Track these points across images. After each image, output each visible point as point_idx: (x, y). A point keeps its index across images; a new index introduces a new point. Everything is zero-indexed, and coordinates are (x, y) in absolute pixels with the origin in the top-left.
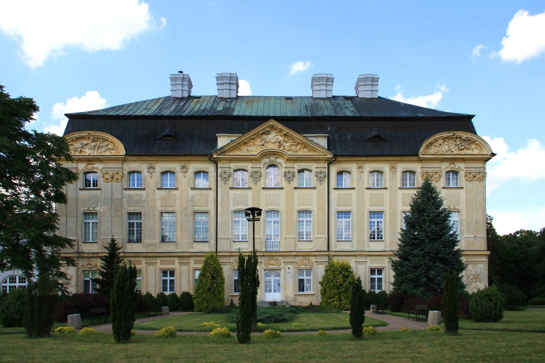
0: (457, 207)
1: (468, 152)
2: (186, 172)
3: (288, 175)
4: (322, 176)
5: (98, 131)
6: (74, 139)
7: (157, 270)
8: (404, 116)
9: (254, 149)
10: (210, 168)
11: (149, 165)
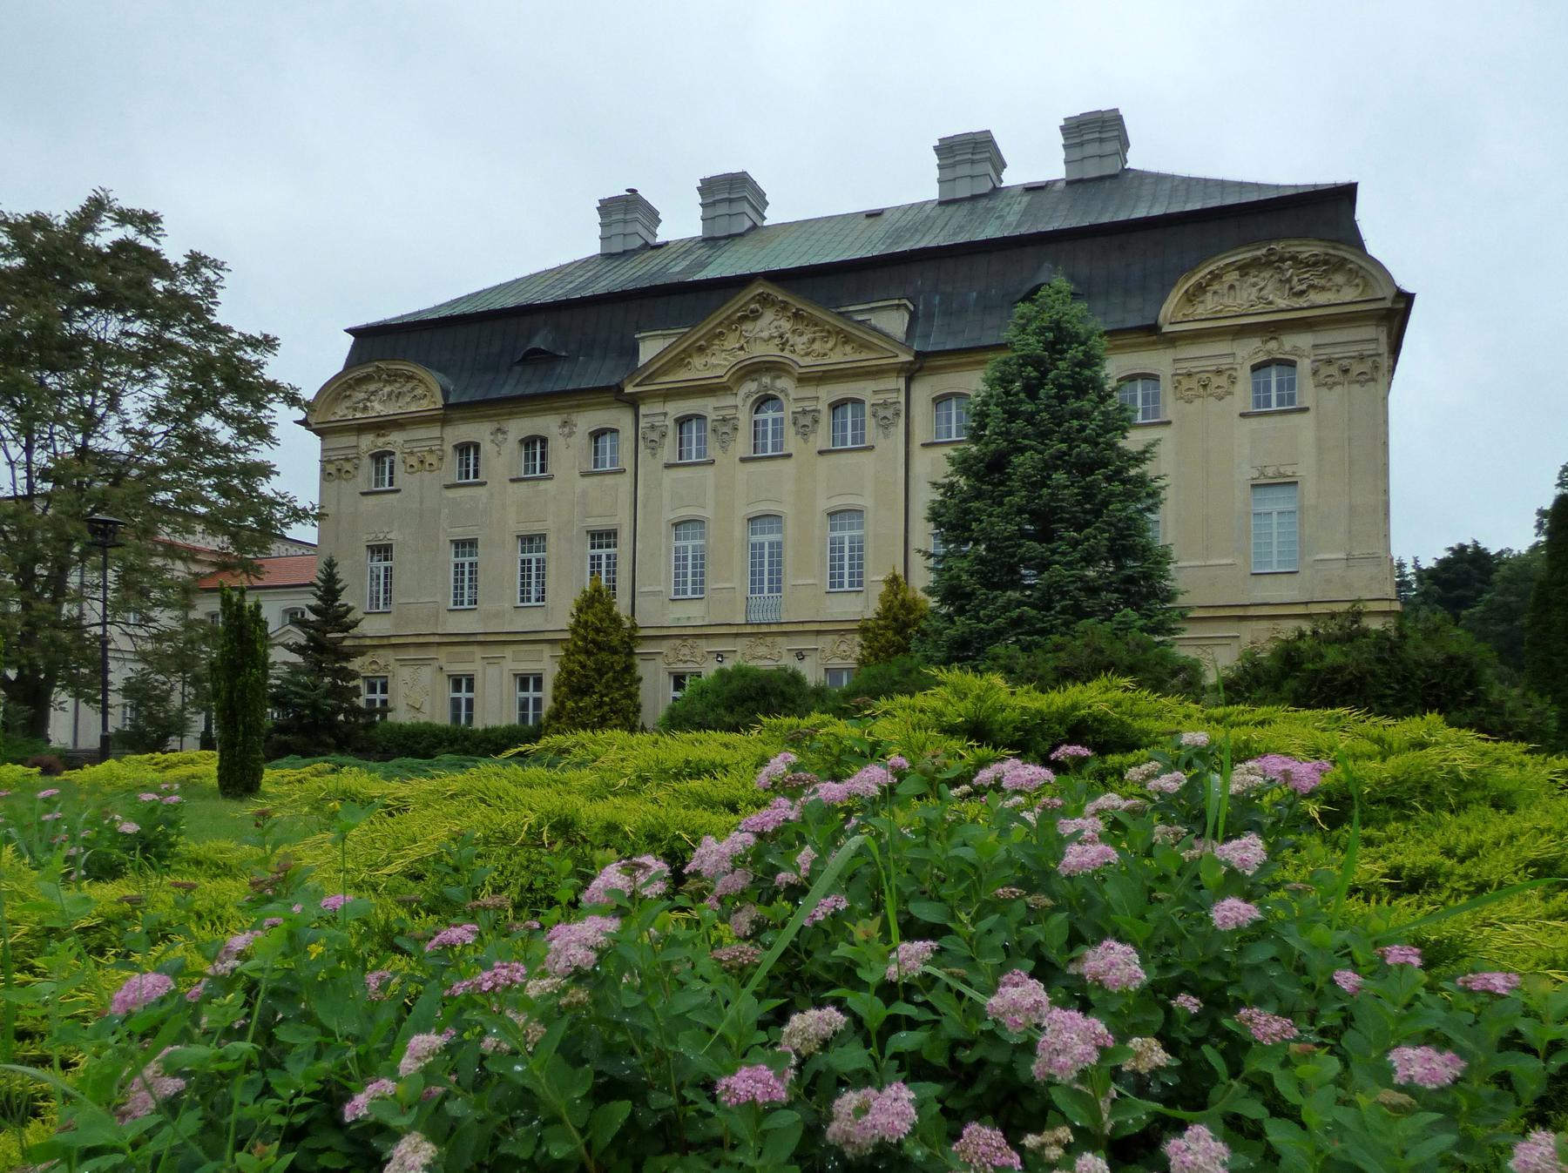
2: (571, 434)
3: (803, 421)
4: (889, 413)
5: (1221, 252)
9: (716, 363)
10: (620, 418)
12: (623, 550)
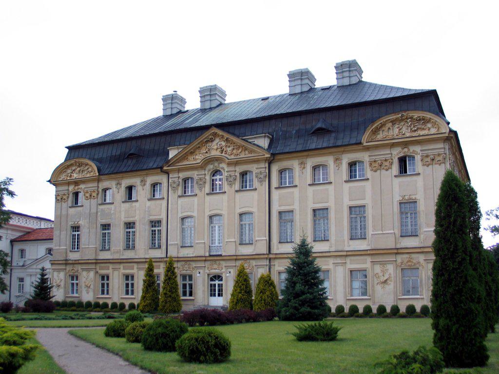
0: (413, 197)
1: (422, 133)
2: (144, 185)
6: (66, 166)
7: (120, 274)
9: (199, 158)
10: (163, 179)
11: (117, 182)
12: (163, 228)
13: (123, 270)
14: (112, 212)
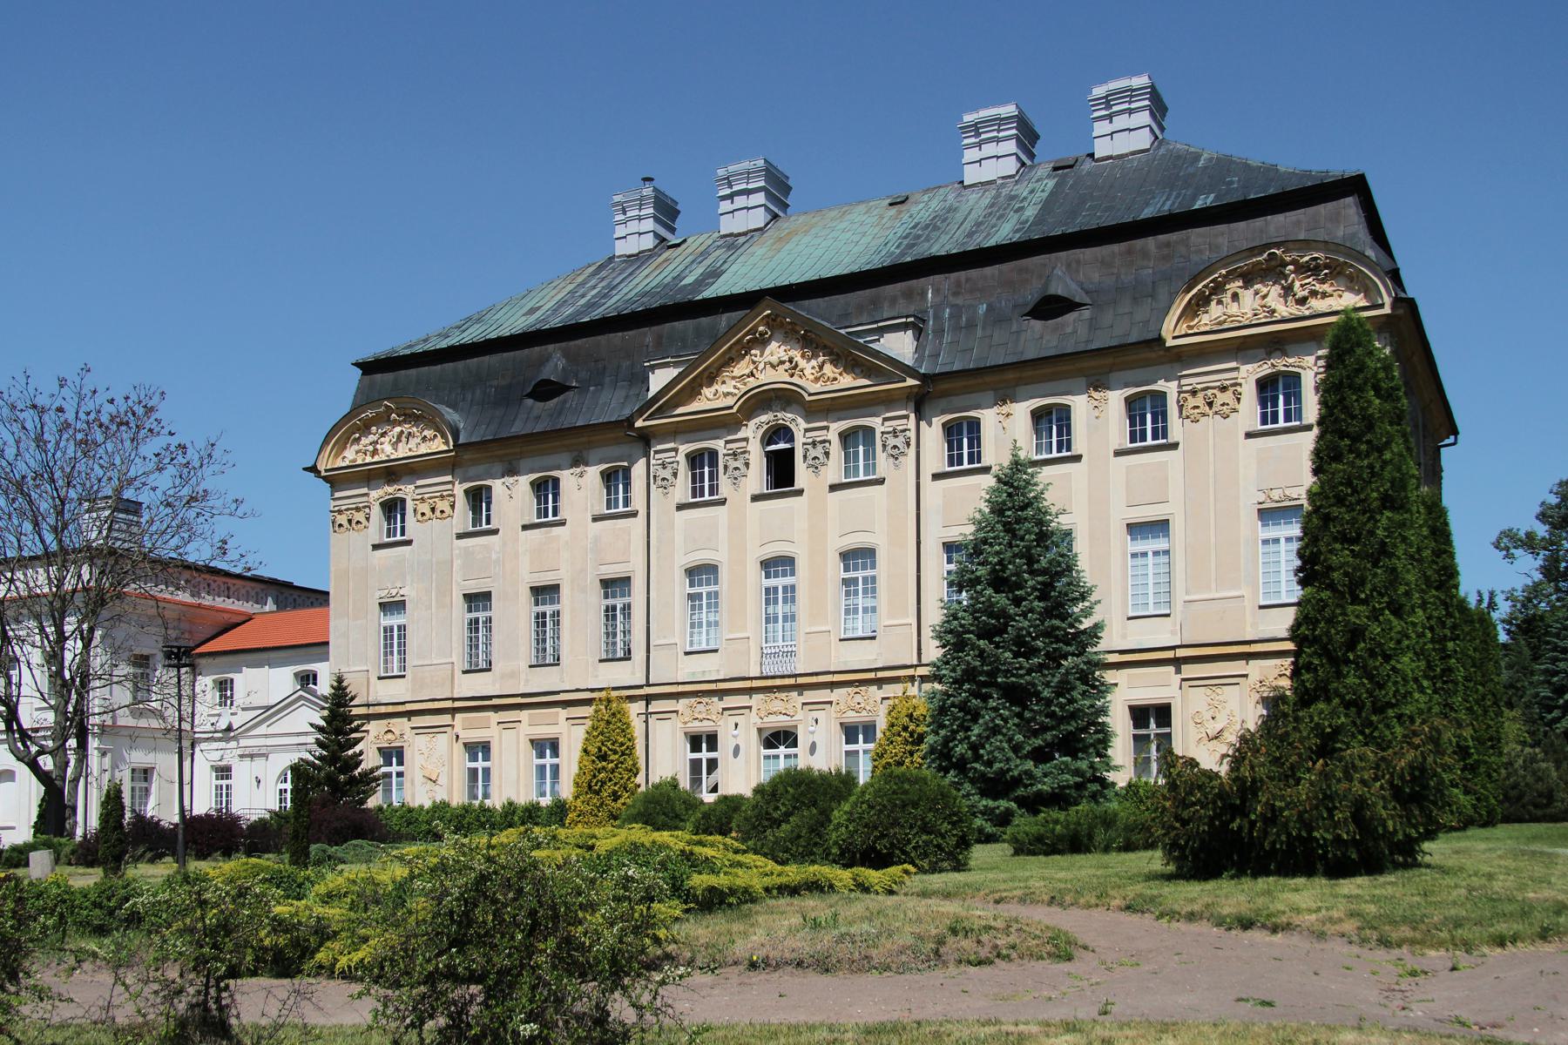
8: (486, 358)
12: (637, 598)
13: (532, 724)
14: (494, 557)
